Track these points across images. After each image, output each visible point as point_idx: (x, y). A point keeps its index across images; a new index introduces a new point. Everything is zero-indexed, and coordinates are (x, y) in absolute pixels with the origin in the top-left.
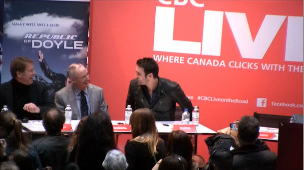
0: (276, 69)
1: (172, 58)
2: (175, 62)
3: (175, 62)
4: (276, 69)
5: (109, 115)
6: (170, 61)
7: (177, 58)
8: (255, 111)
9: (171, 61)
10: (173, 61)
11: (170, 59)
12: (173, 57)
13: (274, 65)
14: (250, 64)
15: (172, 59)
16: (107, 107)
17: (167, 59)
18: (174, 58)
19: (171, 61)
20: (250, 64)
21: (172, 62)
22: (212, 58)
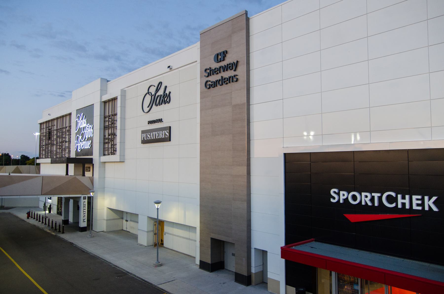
0: (376, 204)
1: (417, 199)
2: (427, 208)
3: (427, 208)
4: (376, 204)
5: (18, 216)
6: (415, 207)
7: (366, 197)
8: (268, 252)
9: (418, 205)
10: (423, 205)
11: (415, 202)
12: (419, 197)
13: (373, 194)
14: (429, 199)
15: (420, 202)
16: (59, 223)
17: (407, 201)
18: (423, 200)
19: (418, 205)
20: (429, 199)
21: (420, 208)
22: (36, 162)
